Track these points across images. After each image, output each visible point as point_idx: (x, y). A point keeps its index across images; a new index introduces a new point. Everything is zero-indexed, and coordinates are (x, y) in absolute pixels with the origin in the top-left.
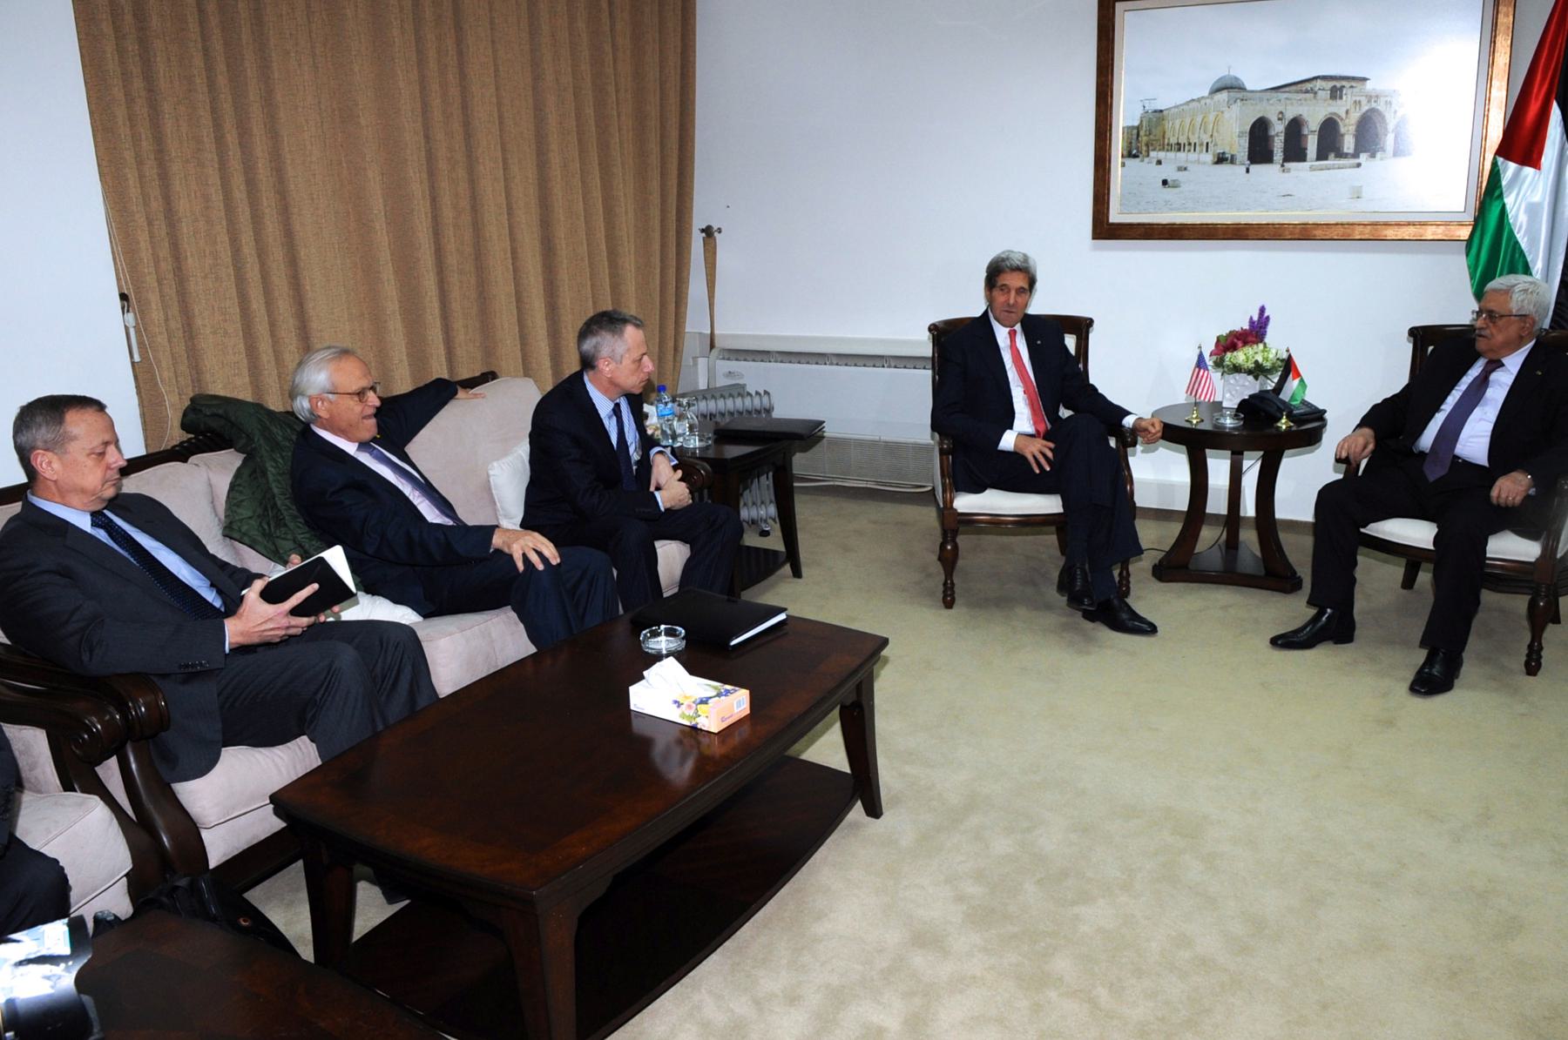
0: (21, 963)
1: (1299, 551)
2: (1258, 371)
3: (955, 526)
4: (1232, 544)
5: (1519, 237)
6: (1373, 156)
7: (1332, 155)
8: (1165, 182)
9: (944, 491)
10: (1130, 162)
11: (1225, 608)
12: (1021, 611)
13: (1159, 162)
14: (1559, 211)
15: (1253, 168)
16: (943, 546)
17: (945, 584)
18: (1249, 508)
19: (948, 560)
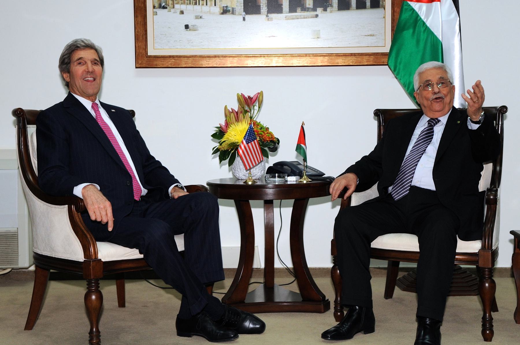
0: (302, 128)
6: (325, 10)
7: (299, 9)
8: (187, 27)
10: (160, 12)
13: (182, 12)
15: (248, 17)
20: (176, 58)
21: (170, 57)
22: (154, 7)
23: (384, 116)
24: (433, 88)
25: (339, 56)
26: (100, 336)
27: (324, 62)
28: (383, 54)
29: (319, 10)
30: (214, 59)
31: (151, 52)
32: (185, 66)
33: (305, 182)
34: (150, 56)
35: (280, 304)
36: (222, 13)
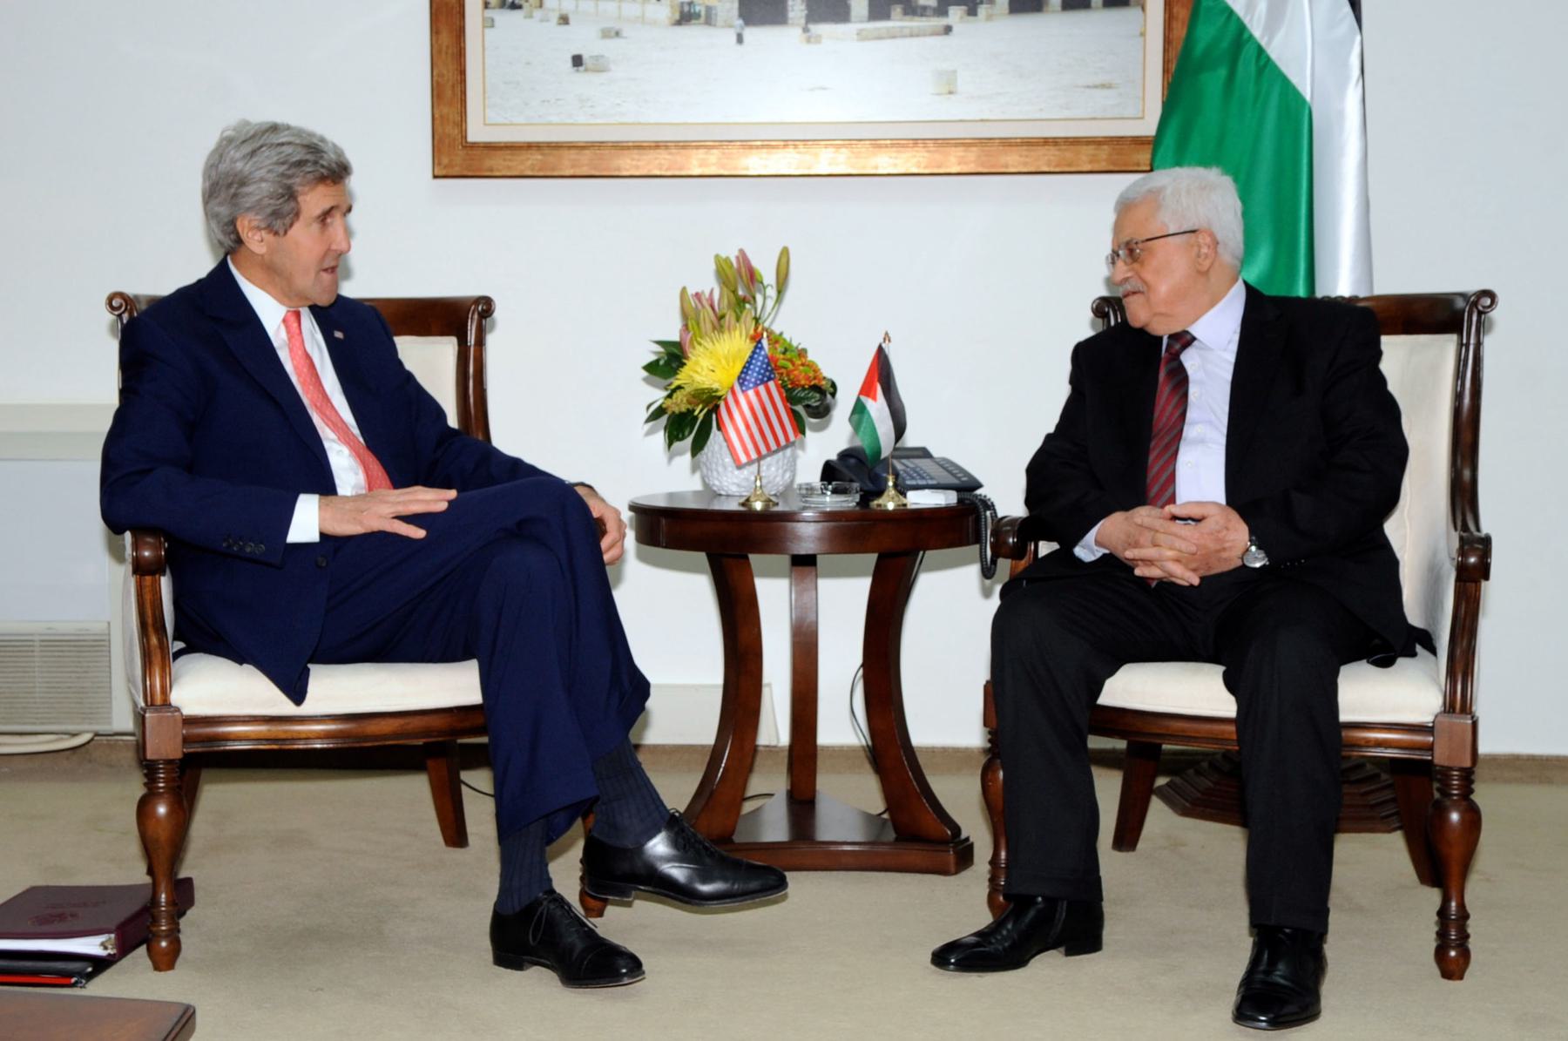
1: (962, 800)
4: (802, 804)
7: (897, 10)
8: (577, 61)
15: (751, 33)
22: (486, 5)
25: (1010, 145)
28: (1138, 141)
29: (956, 14)
30: (652, 154)
34: (474, 146)
36: (679, 23)
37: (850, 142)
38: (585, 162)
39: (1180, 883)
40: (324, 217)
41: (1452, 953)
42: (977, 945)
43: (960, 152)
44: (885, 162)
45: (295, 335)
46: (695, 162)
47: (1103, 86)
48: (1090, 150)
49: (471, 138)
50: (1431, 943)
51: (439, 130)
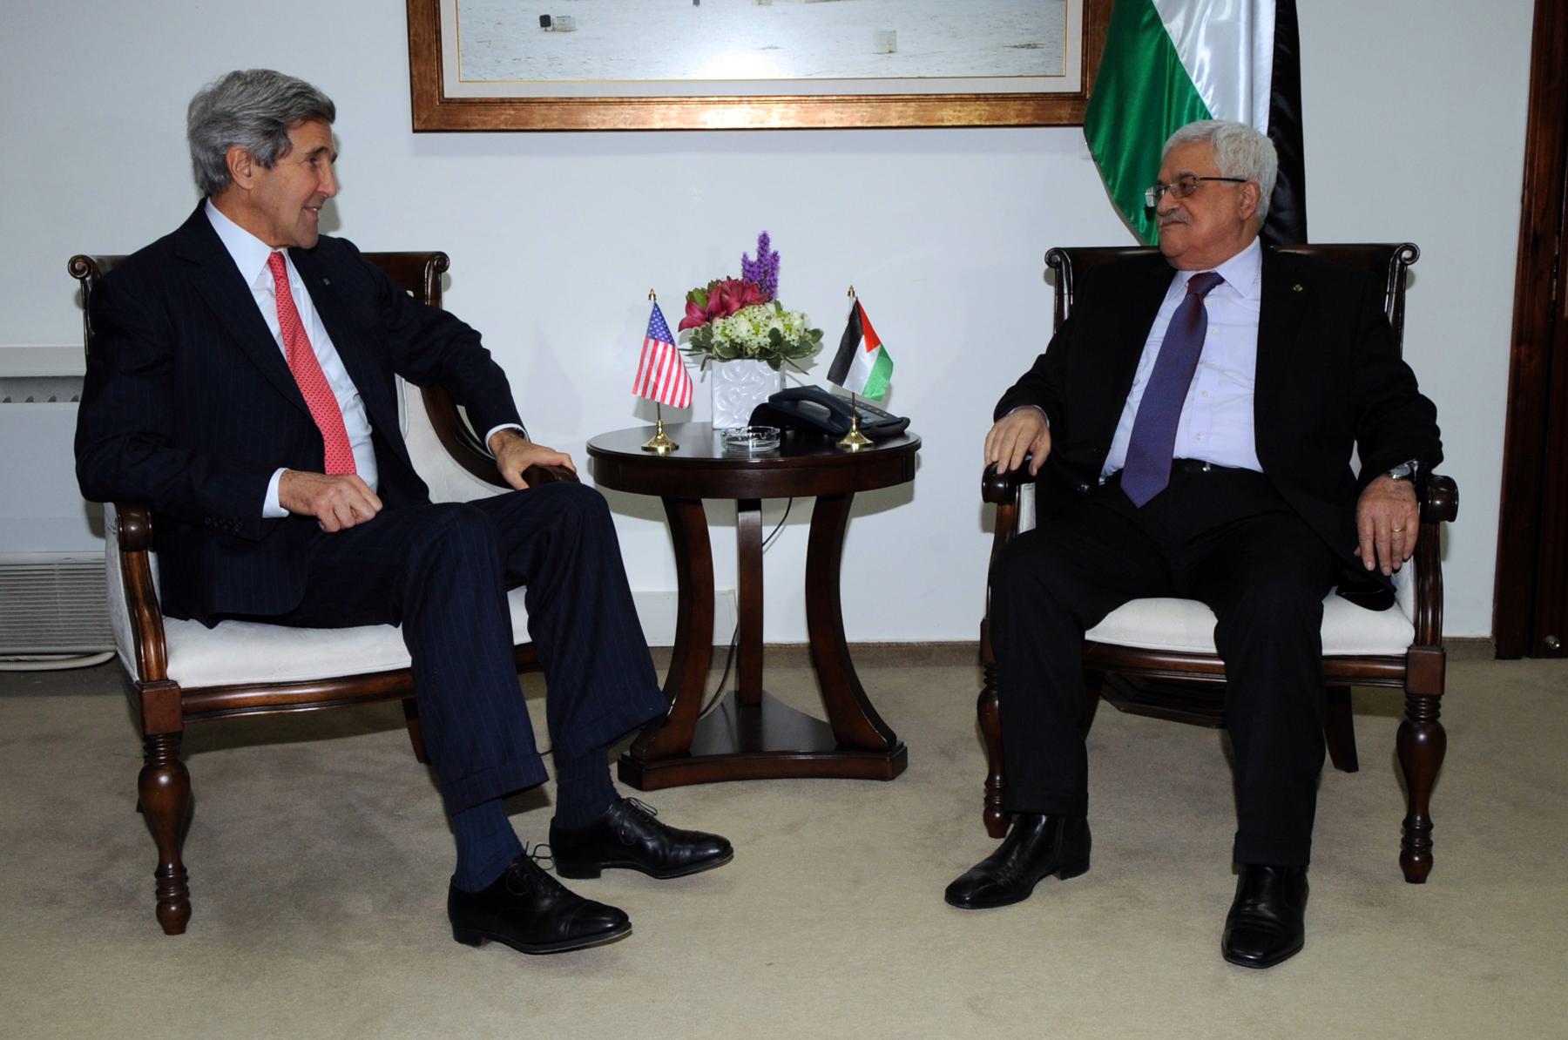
2: (776, 352)
3: (149, 693)
5: (1199, 86)
8: (545, 21)
9: (139, 639)
11: (791, 828)
12: (361, 905)
14: (1256, 44)
16: (146, 780)
17: (161, 873)
18: (785, 623)
19: (169, 818)
20: (519, 106)
21: (502, 102)
23: (1075, 268)
24: (1158, 197)
25: (946, 100)
26: (187, 879)
27: (788, 119)
28: (1060, 97)
30: (617, 109)
31: (452, 90)
32: (897, 123)
33: (855, 447)
34: (451, 101)
35: (793, 757)
37: (801, 99)
38: (555, 117)
39: (1160, 800)
40: (313, 157)
41: (1416, 862)
42: (983, 881)
43: (899, 106)
44: (831, 116)
45: (281, 279)
46: (657, 116)
47: (1028, 46)
48: (1017, 105)
49: (447, 95)
50: (1395, 852)
51: (418, 86)
